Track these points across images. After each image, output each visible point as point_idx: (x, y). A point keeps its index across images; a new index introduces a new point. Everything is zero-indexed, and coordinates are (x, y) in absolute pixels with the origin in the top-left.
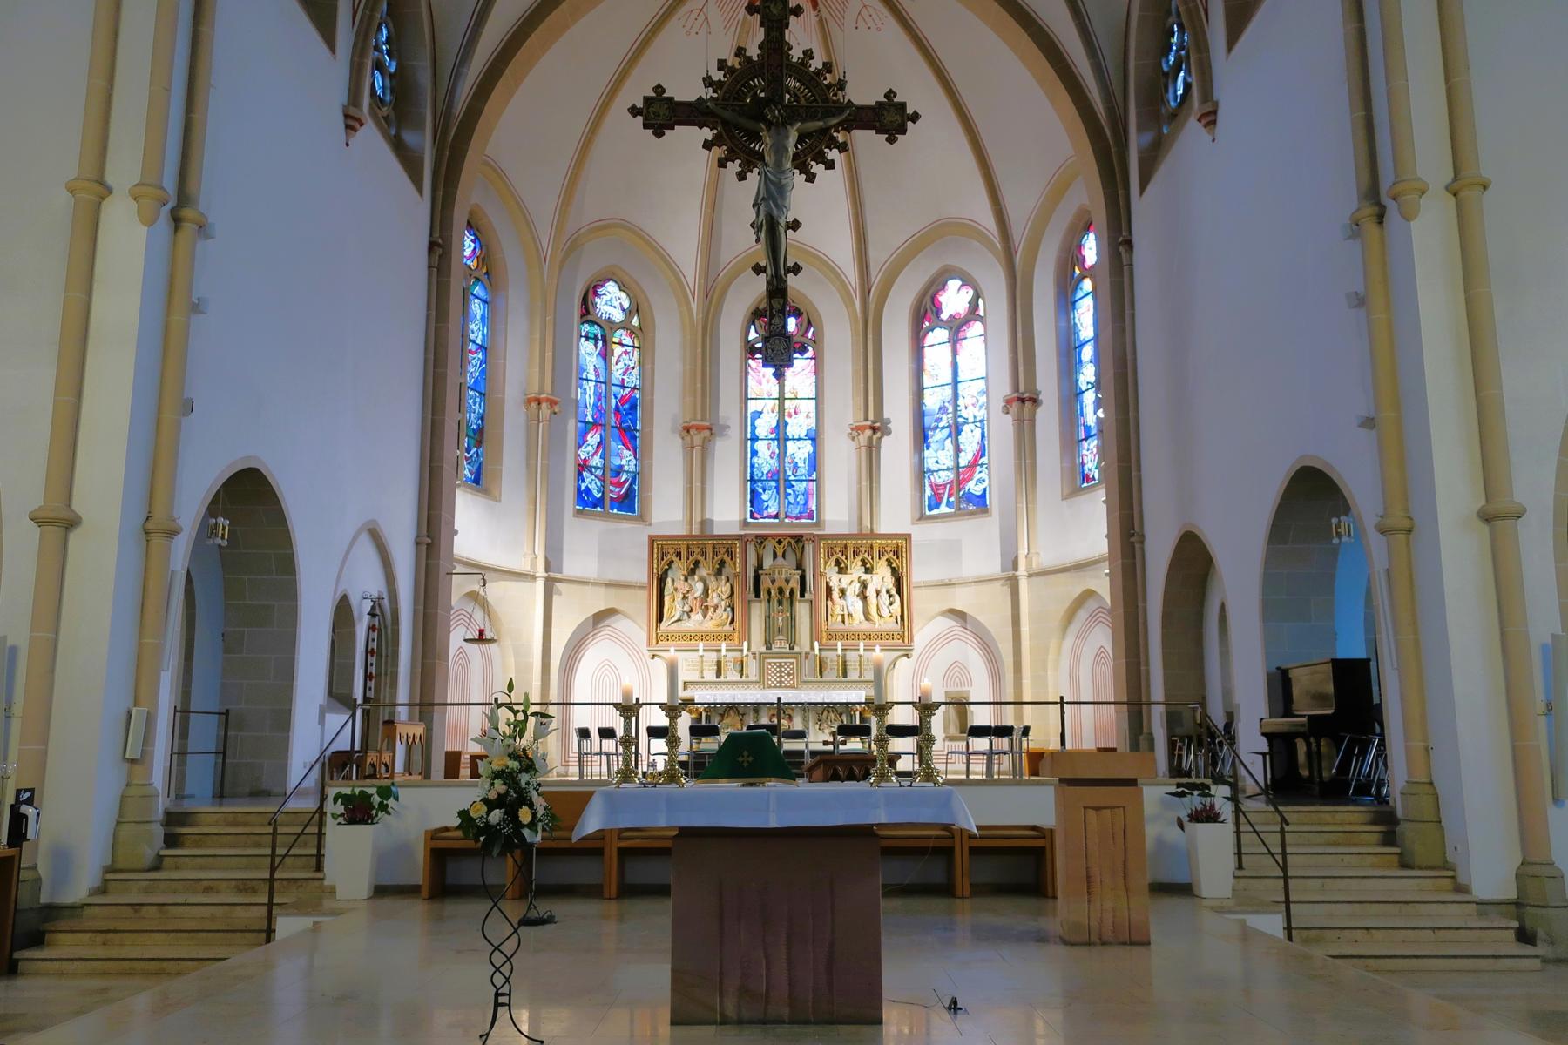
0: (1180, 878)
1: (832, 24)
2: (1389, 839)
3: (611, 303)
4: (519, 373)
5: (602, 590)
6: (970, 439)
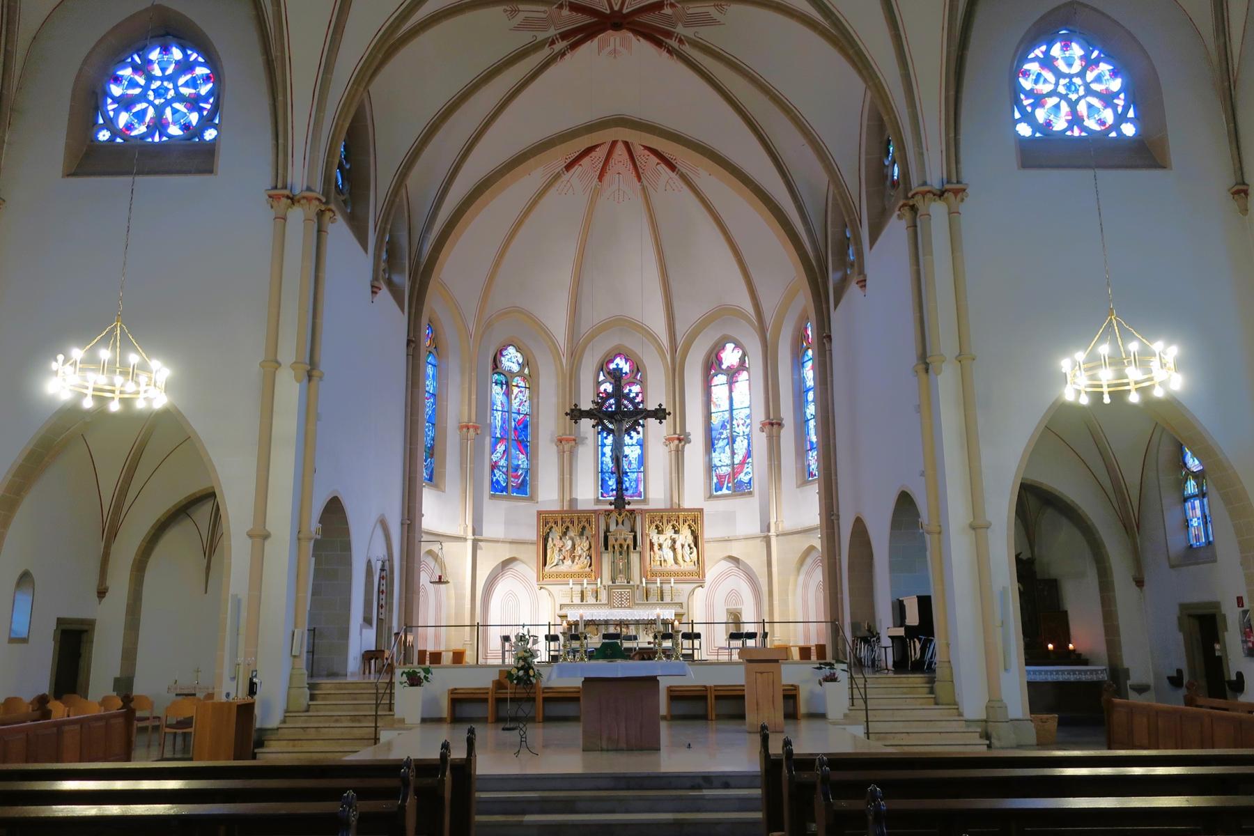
0: (821, 711)
1: (651, 190)
2: (932, 691)
3: (512, 359)
4: (456, 409)
5: (508, 546)
6: (741, 446)
